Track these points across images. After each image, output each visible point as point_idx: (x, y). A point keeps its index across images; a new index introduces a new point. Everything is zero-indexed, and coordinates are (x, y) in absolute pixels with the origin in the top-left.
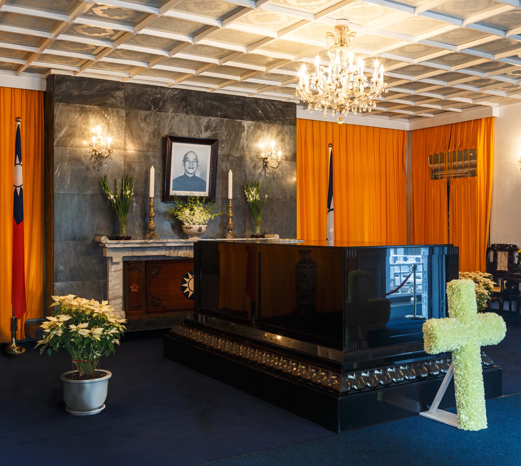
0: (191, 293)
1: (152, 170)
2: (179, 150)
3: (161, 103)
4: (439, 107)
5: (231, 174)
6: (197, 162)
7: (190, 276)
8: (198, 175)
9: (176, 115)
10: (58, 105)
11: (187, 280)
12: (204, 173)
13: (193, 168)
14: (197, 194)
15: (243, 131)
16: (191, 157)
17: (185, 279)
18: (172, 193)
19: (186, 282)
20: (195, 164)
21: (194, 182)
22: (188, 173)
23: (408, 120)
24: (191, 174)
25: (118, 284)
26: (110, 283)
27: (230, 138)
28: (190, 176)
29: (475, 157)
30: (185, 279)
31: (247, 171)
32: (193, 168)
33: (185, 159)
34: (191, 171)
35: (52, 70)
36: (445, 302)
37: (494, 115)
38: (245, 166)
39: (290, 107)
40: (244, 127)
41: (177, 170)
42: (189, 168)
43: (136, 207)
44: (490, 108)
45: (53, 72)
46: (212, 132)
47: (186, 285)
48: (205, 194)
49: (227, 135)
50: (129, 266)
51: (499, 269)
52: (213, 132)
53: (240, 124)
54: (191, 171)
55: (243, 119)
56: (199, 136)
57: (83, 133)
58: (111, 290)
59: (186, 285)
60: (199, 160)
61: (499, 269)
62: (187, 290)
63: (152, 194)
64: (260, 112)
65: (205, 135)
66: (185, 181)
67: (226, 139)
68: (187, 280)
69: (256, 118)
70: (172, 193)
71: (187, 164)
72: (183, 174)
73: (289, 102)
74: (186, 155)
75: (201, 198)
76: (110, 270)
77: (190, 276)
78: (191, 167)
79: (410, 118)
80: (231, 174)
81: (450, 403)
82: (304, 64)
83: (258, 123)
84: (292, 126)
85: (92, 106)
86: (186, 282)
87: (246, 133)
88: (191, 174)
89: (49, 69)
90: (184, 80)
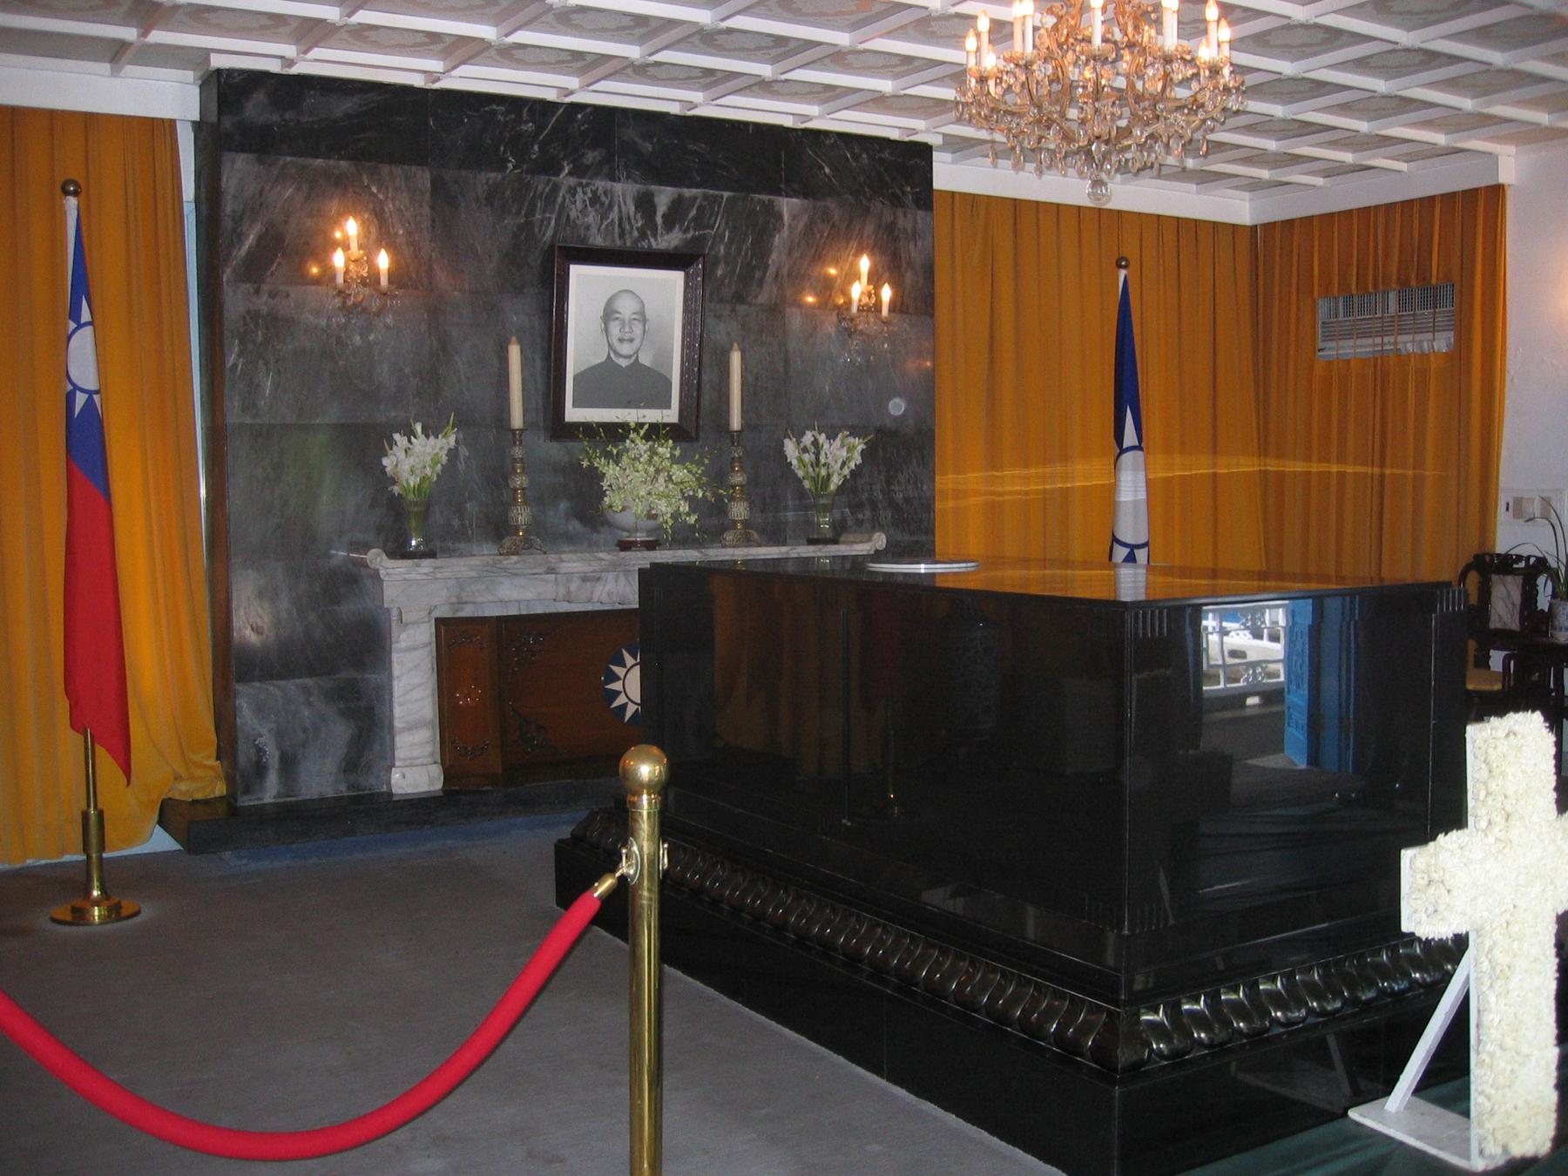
1: (514, 353)
2: (588, 286)
3: (536, 148)
4: (1348, 157)
5: (736, 358)
6: (644, 321)
7: (629, 660)
8: (646, 360)
9: (580, 184)
10: (233, 162)
11: (619, 671)
12: (664, 355)
14: (652, 416)
15: (777, 228)
16: (626, 307)
17: (615, 704)
18: (573, 414)
19: (617, 693)
21: (638, 383)
22: (616, 353)
23: (1247, 195)
24: (626, 357)
25: (420, 685)
26: (395, 683)
27: (739, 251)
28: (624, 363)
30: (615, 704)
31: (792, 345)
32: (631, 340)
33: (609, 314)
34: (626, 349)
35: (213, 57)
37: (1502, 180)
39: (911, 161)
40: (781, 217)
42: (621, 340)
44: (1492, 157)
45: (217, 62)
46: (686, 231)
47: (617, 686)
48: (671, 415)
50: (455, 637)
51: (1495, 623)
52: (690, 234)
53: (769, 209)
54: (626, 349)
55: (778, 192)
57: (307, 243)
58: (401, 705)
59: (617, 686)
61: (1495, 623)
62: (621, 700)
63: (517, 420)
64: (827, 170)
65: (669, 240)
66: (609, 381)
67: (727, 254)
68: (619, 671)
70: (573, 414)
71: (615, 329)
72: (602, 358)
73: (911, 142)
75: (654, 432)
76: (394, 646)
77: (629, 660)
78: (627, 336)
79: (1254, 186)
80: (736, 358)
81: (1450, 1076)
82: (638, 446)
83: (820, 204)
84: (920, 213)
85: (331, 162)
86: (617, 693)
87: (785, 232)
88: (626, 357)
89: (206, 53)
90: (604, 78)
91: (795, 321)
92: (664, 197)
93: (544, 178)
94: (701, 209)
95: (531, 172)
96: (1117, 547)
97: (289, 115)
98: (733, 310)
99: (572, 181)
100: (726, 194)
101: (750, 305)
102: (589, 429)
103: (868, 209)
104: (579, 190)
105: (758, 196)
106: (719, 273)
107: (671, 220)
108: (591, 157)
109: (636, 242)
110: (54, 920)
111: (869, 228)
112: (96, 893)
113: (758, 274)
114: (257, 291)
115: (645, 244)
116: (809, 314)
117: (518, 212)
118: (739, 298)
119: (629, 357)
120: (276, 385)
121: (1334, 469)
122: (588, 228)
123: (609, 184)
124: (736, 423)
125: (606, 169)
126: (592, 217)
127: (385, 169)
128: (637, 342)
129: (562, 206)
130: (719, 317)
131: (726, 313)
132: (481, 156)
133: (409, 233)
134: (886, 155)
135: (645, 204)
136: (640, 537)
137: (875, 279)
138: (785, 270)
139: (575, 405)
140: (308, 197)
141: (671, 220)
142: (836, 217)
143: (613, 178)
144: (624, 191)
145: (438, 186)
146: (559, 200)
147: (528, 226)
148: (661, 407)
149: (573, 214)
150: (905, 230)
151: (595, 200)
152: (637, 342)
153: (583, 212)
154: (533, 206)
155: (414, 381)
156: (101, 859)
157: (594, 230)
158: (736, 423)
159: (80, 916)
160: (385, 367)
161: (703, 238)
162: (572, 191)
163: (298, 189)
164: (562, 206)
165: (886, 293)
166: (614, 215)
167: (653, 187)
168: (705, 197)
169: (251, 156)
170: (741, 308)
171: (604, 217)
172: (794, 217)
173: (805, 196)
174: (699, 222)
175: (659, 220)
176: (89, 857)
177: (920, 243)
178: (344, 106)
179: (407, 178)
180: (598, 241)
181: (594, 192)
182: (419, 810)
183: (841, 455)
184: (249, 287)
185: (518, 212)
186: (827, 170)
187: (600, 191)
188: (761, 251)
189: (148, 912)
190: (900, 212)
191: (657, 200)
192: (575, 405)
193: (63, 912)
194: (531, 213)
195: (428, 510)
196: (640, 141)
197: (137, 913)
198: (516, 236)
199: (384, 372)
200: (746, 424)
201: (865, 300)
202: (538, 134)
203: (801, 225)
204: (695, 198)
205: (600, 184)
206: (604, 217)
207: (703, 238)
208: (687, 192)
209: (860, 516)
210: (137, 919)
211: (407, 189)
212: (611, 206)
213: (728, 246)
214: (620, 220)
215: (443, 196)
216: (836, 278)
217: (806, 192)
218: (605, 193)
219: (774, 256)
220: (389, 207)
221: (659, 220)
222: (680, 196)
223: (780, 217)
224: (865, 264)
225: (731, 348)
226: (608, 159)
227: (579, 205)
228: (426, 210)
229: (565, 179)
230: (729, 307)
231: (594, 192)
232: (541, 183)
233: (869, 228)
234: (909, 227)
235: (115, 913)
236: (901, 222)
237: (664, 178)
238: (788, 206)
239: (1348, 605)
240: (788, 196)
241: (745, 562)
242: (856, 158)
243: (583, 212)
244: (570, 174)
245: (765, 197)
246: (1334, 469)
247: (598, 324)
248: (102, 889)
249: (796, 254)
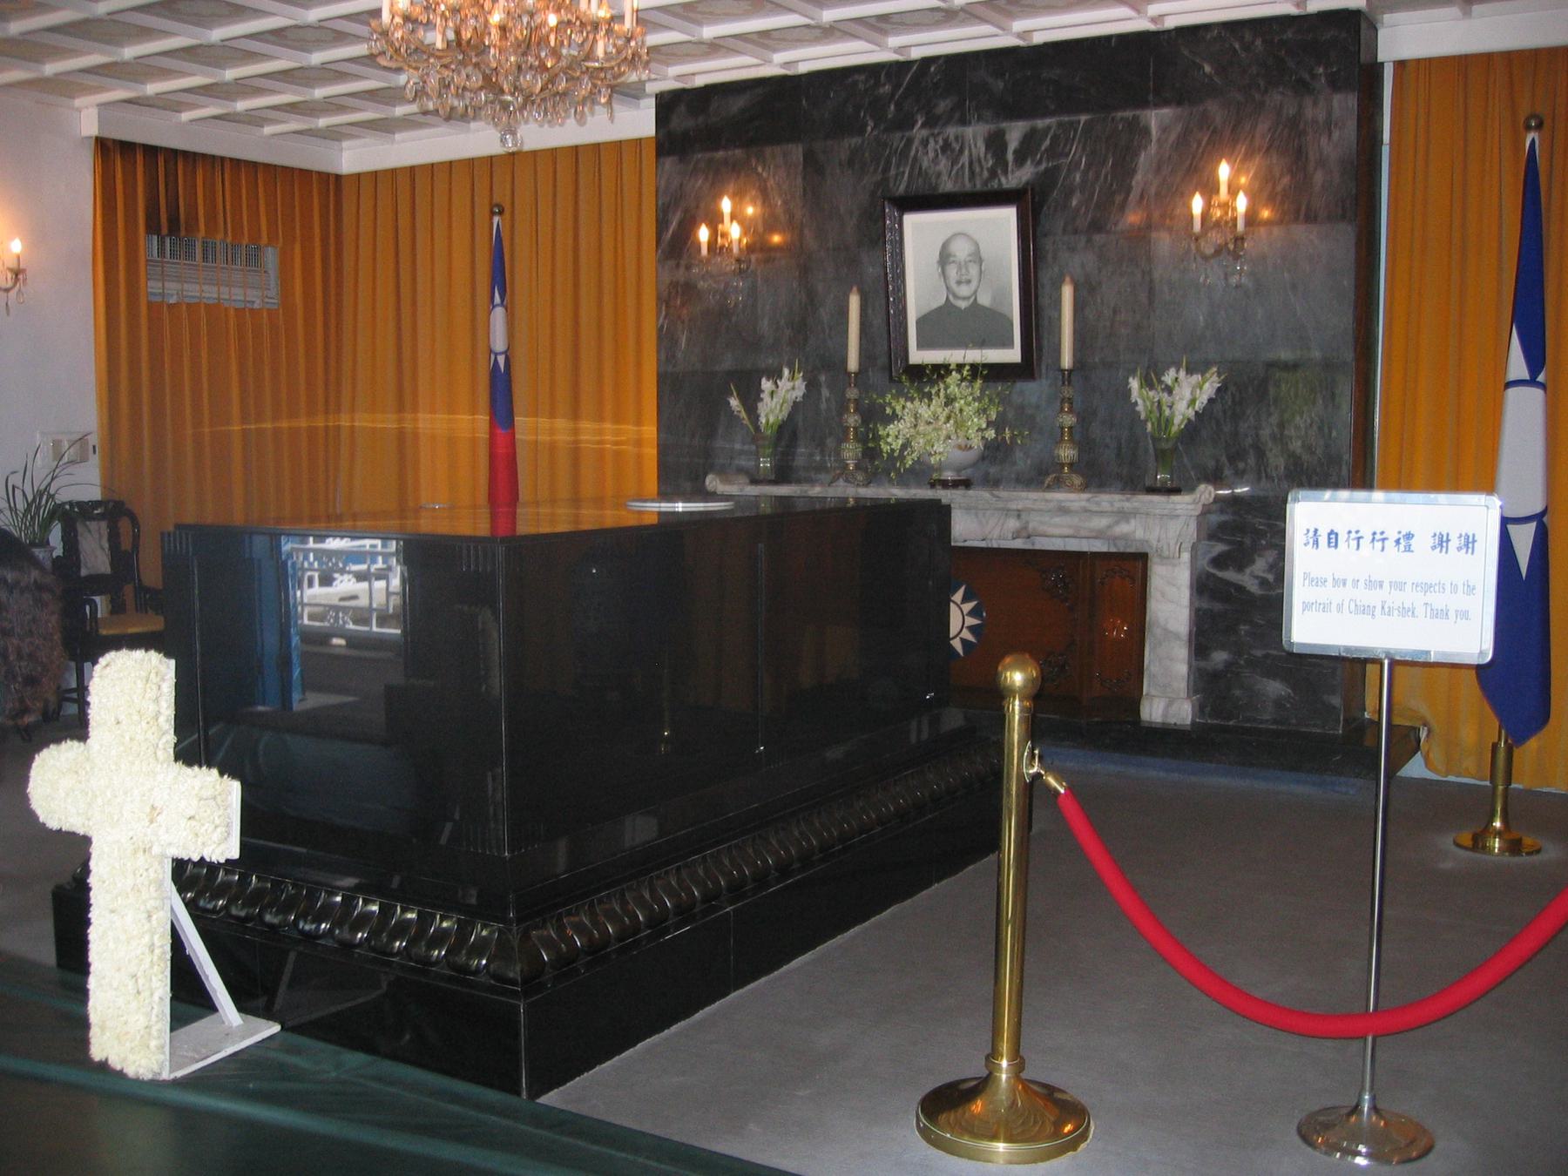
0: (958, 596)
2: (922, 232)
6: (980, 261)
8: (985, 300)
13: (969, 282)
16: (961, 250)
20: (974, 271)
22: (956, 296)
24: (964, 298)
28: (963, 305)
29: (214, 309)
31: (1156, 275)
32: (969, 282)
33: (945, 258)
34: (964, 291)
36: (559, 214)
38: (1149, 259)
41: (921, 291)
42: (959, 283)
43: (828, 400)
46: (1039, 163)
49: (1088, 165)
52: (1043, 167)
54: (964, 291)
55: (1144, 104)
56: (1000, 183)
60: (983, 255)
62: (968, 607)
64: (1207, 69)
66: (947, 324)
67: (1084, 181)
69: (1182, 94)
70: (917, 356)
71: (952, 271)
74: (945, 246)
87: (1153, 148)
88: (964, 298)
92: (1015, 133)
93: (898, 135)
94: (1055, 139)
95: (886, 130)
96: (1511, 528)
97: (701, 119)
98: (1089, 241)
99: (925, 132)
100: (1083, 118)
101: (1108, 232)
103: (1262, 104)
104: (932, 141)
105: (1120, 114)
106: (1074, 203)
107: (1020, 158)
108: (943, 106)
109: (986, 183)
110: (1458, 845)
111: (1263, 126)
112: (1497, 824)
113: (1118, 199)
114: (678, 266)
115: (995, 184)
117: (876, 170)
118: (1097, 226)
120: (689, 340)
121: (284, 424)
122: (939, 175)
123: (960, 129)
124: (853, 364)
125: (957, 115)
126: (943, 163)
127: (768, 151)
128: (974, 284)
129: (915, 158)
130: (1072, 249)
132: (845, 125)
133: (785, 203)
134: (1289, 35)
135: (996, 143)
136: (949, 475)
138: (1153, 190)
140: (713, 184)
141: (1020, 158)
142: (1218, 120)
143: (964, 122)
144: (974, 134)
145: (809, 157)
146: (913, 153)
147: (885, 180)
149: (925, 164)
150: (1314, 121)
151: (946, 147)
152: (974, 284)
153: (935, 160)
154: (888, 163)
155: (788, 332)
156: (1506, 790)
157: (945, 178)
158: (853, 364)
159: (1479, 843)
160: (766, 322)
161: (1057, 169)
162: (925, 143)
163: (706, 179)
164: (915, 158)
166: (965, 159)
167: (1004, 125)
168: (1060, 125)
169: (675, 158)
170: (1098, 238)
171: (954, 162)
172: (1164, 130)
173: (1179, 103)
174: (1052, 153)
175: (1010, 156)
176: (1494, 788)
177: (1336, 135)
178: (738, 104)
179: (785, 155)
180: (947, 186)
181: (946, 141)
182: (1165, 740)
183: (1188, 394)
184: (672, 263)
185: (876, 170)
186: (1207, 69)
187: (952, 138)
188: (1124, 170)
189: (1551, 852)
190: (1308, 102)
191: (1007, 137)
193: (1466, 839)
194: (886, 170)
196: (990, 80)
197: (1538, 851)
198: (873, 194)
199: (765, 325)
200: (1080, 363)
202: (893, 95)
203: (1173, 137)
204: (1049, 128)
205: (951, 131)
206: (954, 162)
207: (1057, 169)
208: (1041, 123)
209: (1241, 465)
210: (1535, 858)
211: (781, 167)
212: (961, 151)
213: (1085, 173)
214: (971, 163)
215: (813, 166)
217: (1180, 98)
218: (957, 138)
219: (1139, 177)
220: (771, 183)
221: (1010, 156)
222: (1033, 131)
223: (1146, 132)
226: (959, 106)
227: (931, 155)
228: (799, 180)
229: (919, 132)
230: (1083, 239)
231: (946, 141)
232: (897, 140)
233: (1263, 126)
234: (1321, 117)
235: (1514, 847)
236: (1309, 112)
237: (1014, 113)
238: (1156, 118)
240: (1157, 106)
241: (857, 500)
242: (1247, 48)
243: (935, 160)
244: (923, 126)
245: (1128, 114)
246: (284, 424)
247: (935, 269)
248: (1505, 821)
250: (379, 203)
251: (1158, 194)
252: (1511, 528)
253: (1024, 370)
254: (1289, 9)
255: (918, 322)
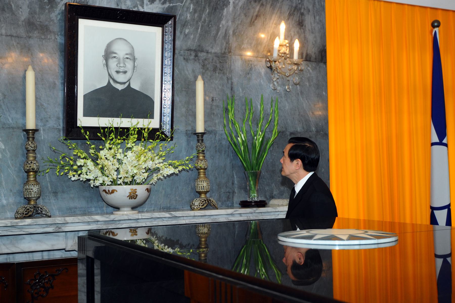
6: (134, 60)
8: (135, 86)
14: (142, 123)
16: (121, 50)
18: (83, 121)
20: (129, 65)
27: (200, 18)
28: (120, 87)
31: (235, 80)
32: (125, 72)
33: (108, 55)
38: (231, 71)
42: (118, 72)
60: (137, 56)
70: (83, 121)
71: (113, 64)
72: (105, 84)
74: (109, 46)
78: (122, 69)
80: (200, 85)
91: (237, 65)
96: (436, 212)
98: (196, 56)
102: (94, 130)
116: (249, 68)
119: (124, 83)
131: (192, 57)
137: (289, 37)
139: (85, 115)
148: (146, 117)
152: (129, 75)
165: (297, 45)
192: (85, 115)
195: (296, 64)
201: (283, 50)
216: (264, 38)
219: (223, 22)
224: (283, 27)
225: (196, 78)
239: (169, 38)
247: (102, 61)
249: (237, 22)
250: (27, 254)
251: (234, 33)
252: (436, 212)
253: (71, 130)
254: (113, 6)
255: (85, 96)
